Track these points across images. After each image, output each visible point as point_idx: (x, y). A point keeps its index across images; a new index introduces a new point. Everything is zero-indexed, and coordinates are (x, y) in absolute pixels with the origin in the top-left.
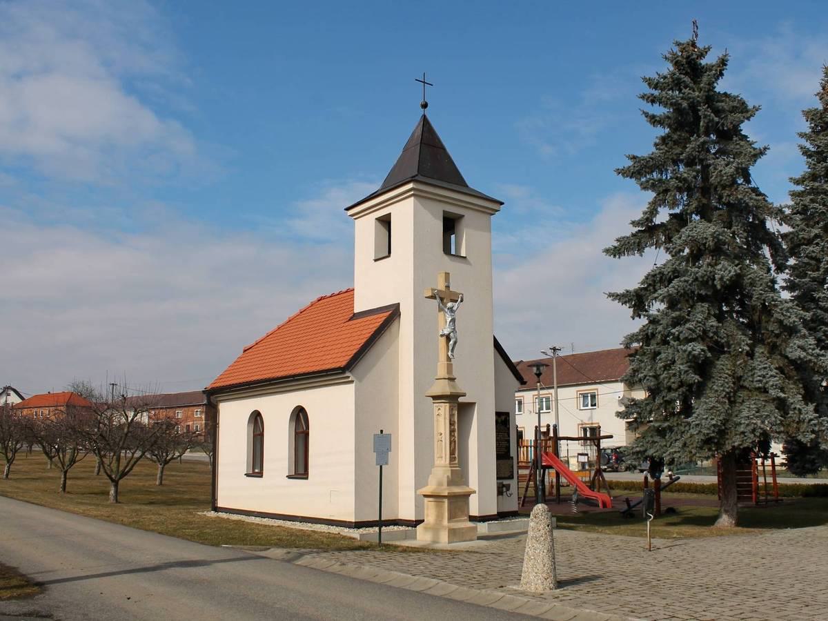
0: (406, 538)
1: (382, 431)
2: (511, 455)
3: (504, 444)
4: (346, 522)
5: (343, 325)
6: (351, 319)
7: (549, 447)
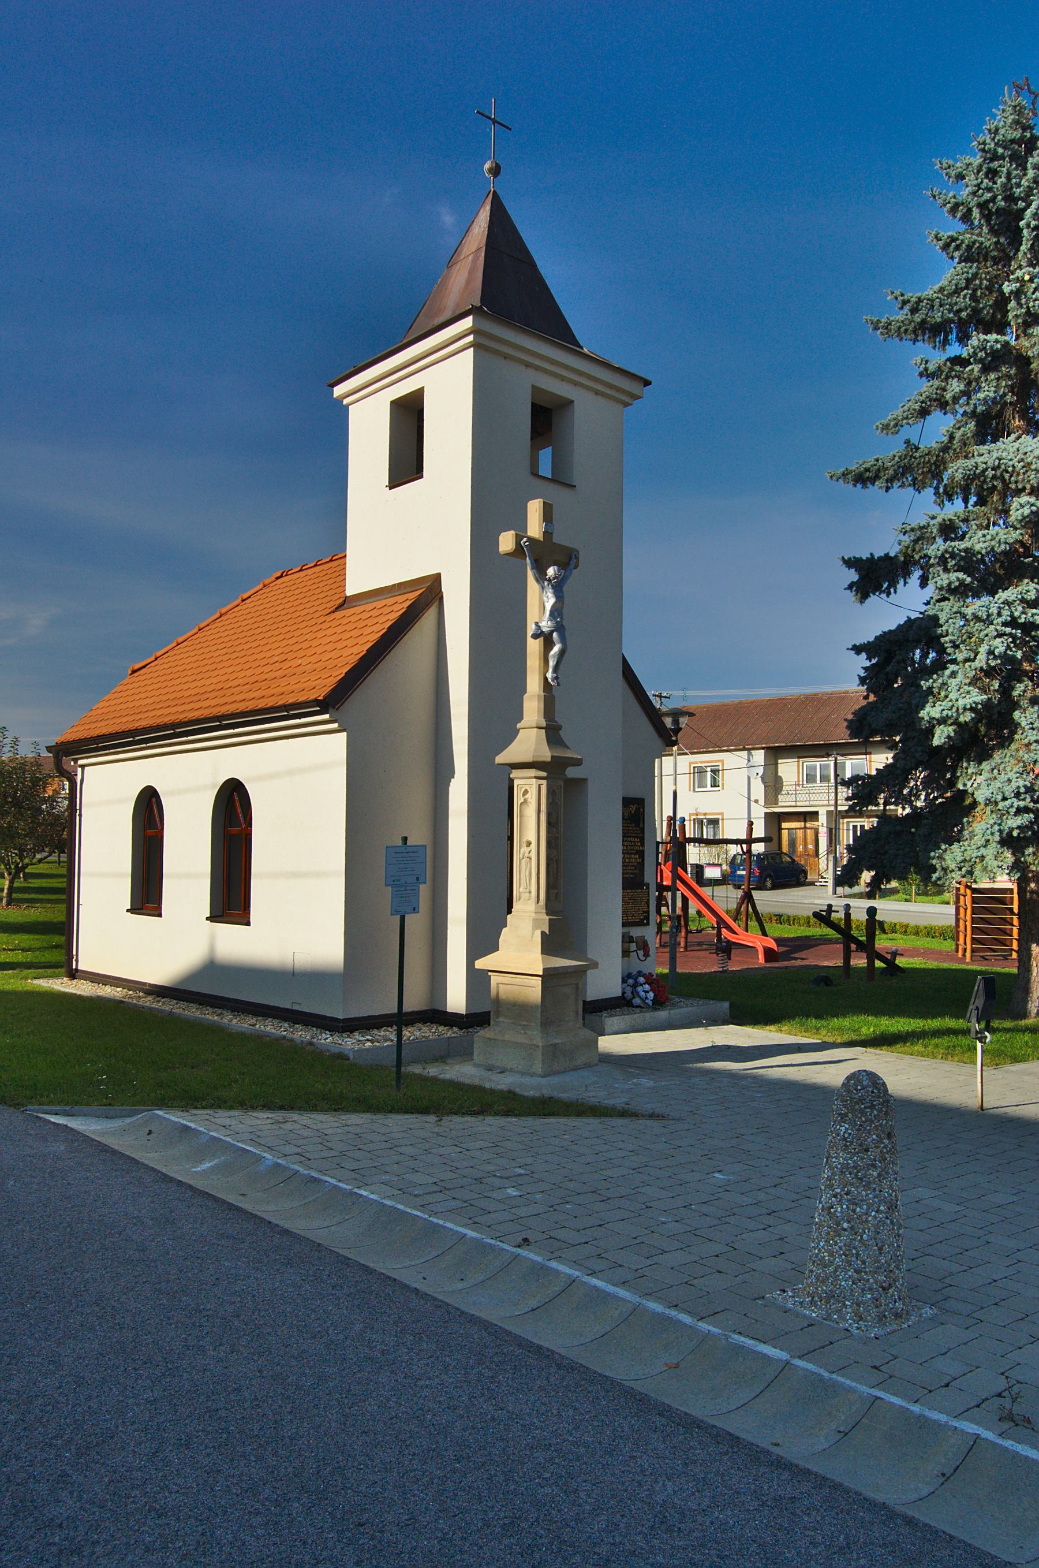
0: (441, 1058)
1: (405, 839)
2: (646, 880)
4: (324, 1017)
5: (323, 619)
6: (339, 608)
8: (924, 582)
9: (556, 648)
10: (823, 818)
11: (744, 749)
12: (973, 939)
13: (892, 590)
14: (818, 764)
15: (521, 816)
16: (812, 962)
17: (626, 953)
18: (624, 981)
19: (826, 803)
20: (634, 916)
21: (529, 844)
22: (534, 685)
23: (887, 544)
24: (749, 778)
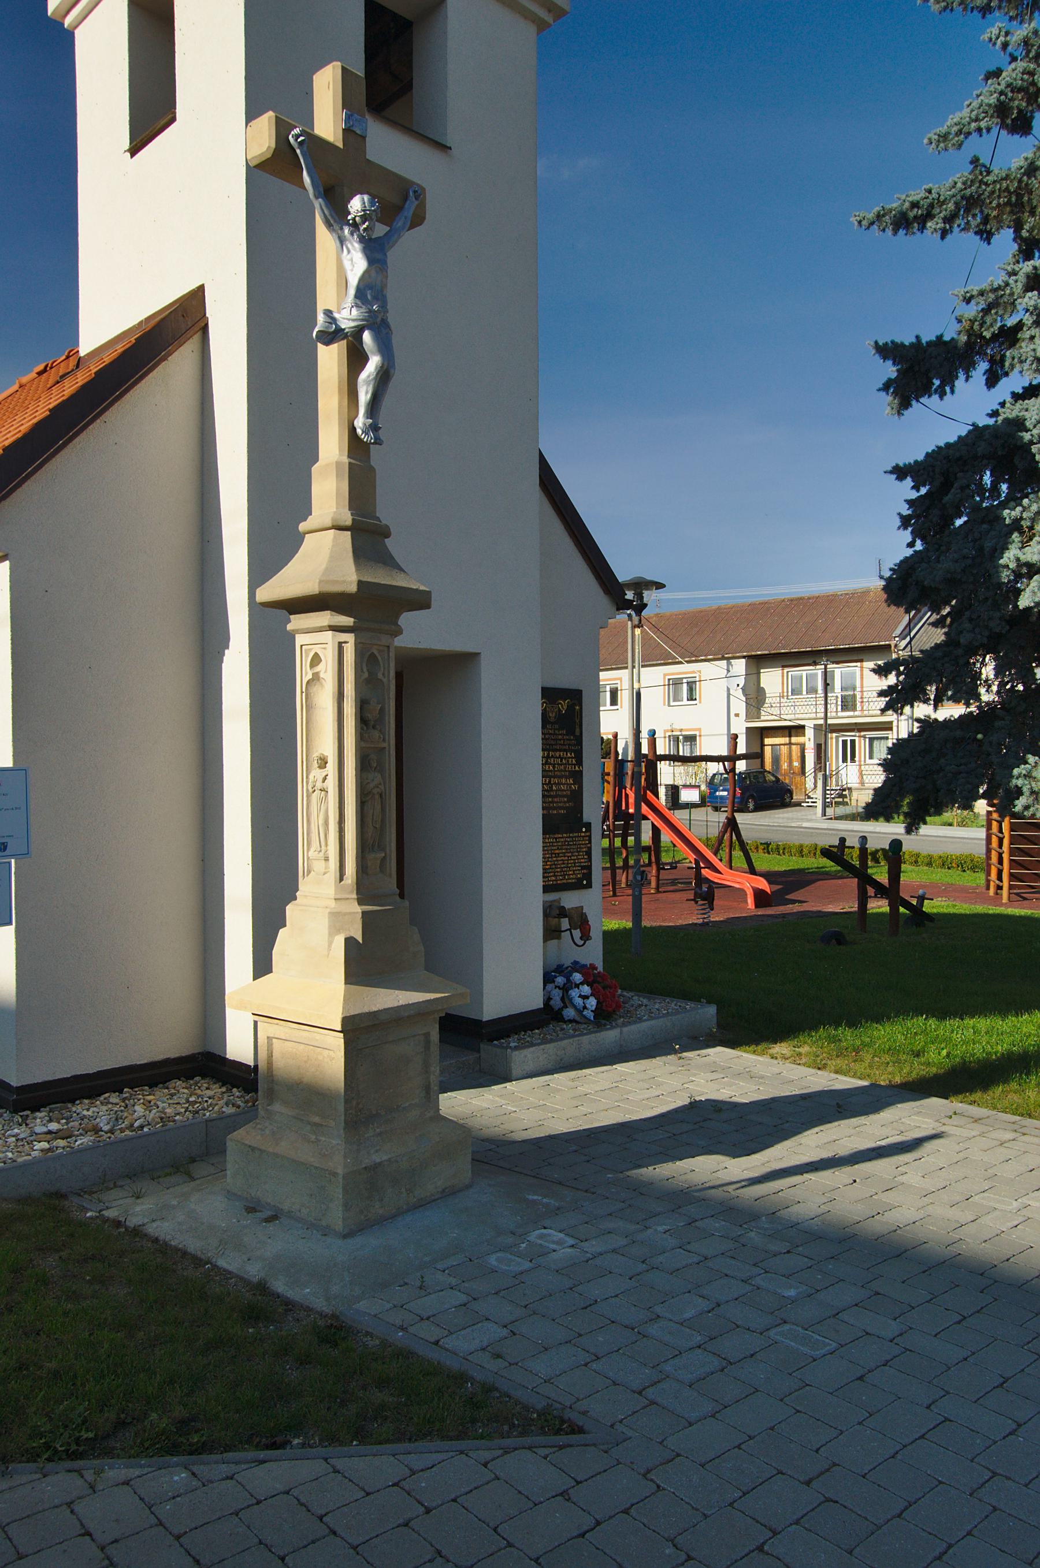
3: (567, 784)
7: (608, 774)
8: (992, 380)
9: (374, 362)
10: (810, 733)
11: (723, 658)
12: (1011, 875)
13: (948, 389)
14: (804, 674)
15: (309, 707)
16: (812, 906)
17: (551, 933)
18: (548, 978)
19: (813, 716)
20: (564, 873)
21: (323, 763)
22: (331, 445)
23: (940, 321)
24: (728, 690)
